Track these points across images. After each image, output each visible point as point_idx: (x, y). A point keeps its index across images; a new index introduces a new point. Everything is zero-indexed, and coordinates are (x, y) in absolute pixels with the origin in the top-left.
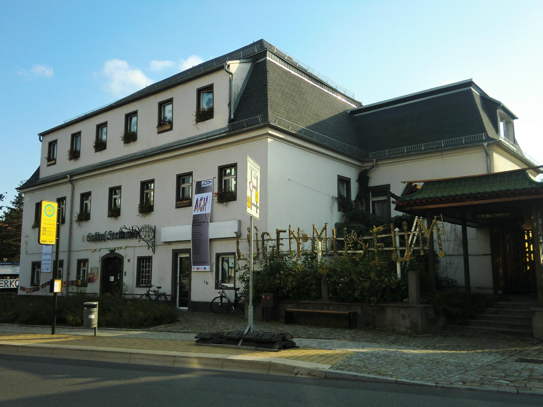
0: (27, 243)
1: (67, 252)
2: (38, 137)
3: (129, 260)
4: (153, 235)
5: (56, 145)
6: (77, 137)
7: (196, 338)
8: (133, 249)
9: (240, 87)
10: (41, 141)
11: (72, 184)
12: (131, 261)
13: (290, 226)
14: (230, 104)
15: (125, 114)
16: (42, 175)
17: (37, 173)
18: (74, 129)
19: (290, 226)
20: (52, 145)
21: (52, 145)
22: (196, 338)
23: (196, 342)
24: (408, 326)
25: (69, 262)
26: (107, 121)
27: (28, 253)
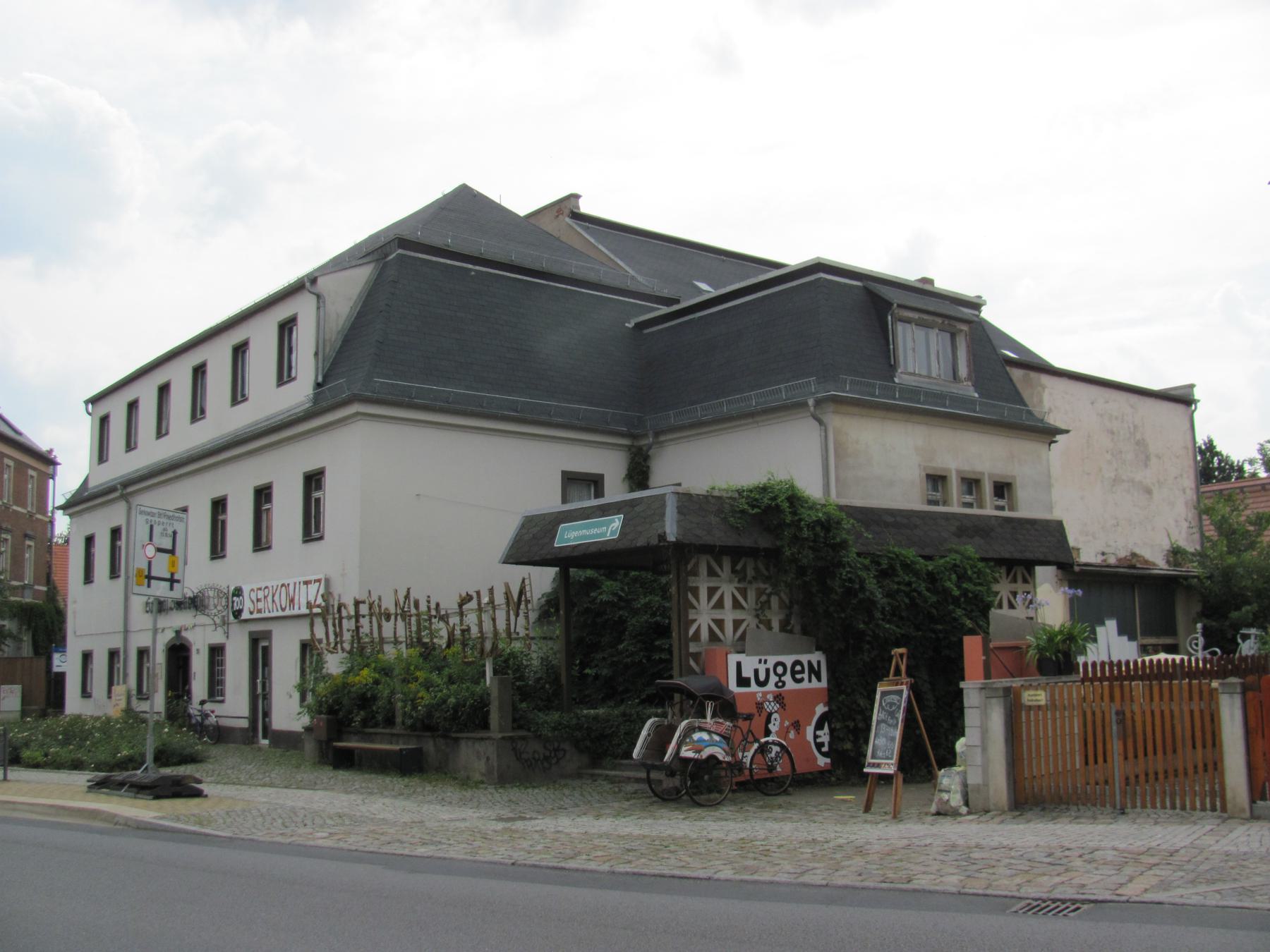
0: (75, 612)
1: (122, 634)
2: (84, 405)
3: (198, 650)
4: (224, 603)
5: (295, 328)
6: (244, 352)
7: (88, 781)
8: (202, 628)
9: (341, 322)
10: (89, 414)
11: (128, 502)
12: (201, 651)
13: (370, 592)
14: (316, 354)
15: (279, 322)
16: (92, 484)
17: (86, 482)
18: (236, 337)
19: (370, 592)
20: (104, 421)
21: (104, 421)
22: (88, 781)
23: (89, 787)
24: (483, 771)
25: (125, 651)
26: (138, 397)
27: (77, 634)
